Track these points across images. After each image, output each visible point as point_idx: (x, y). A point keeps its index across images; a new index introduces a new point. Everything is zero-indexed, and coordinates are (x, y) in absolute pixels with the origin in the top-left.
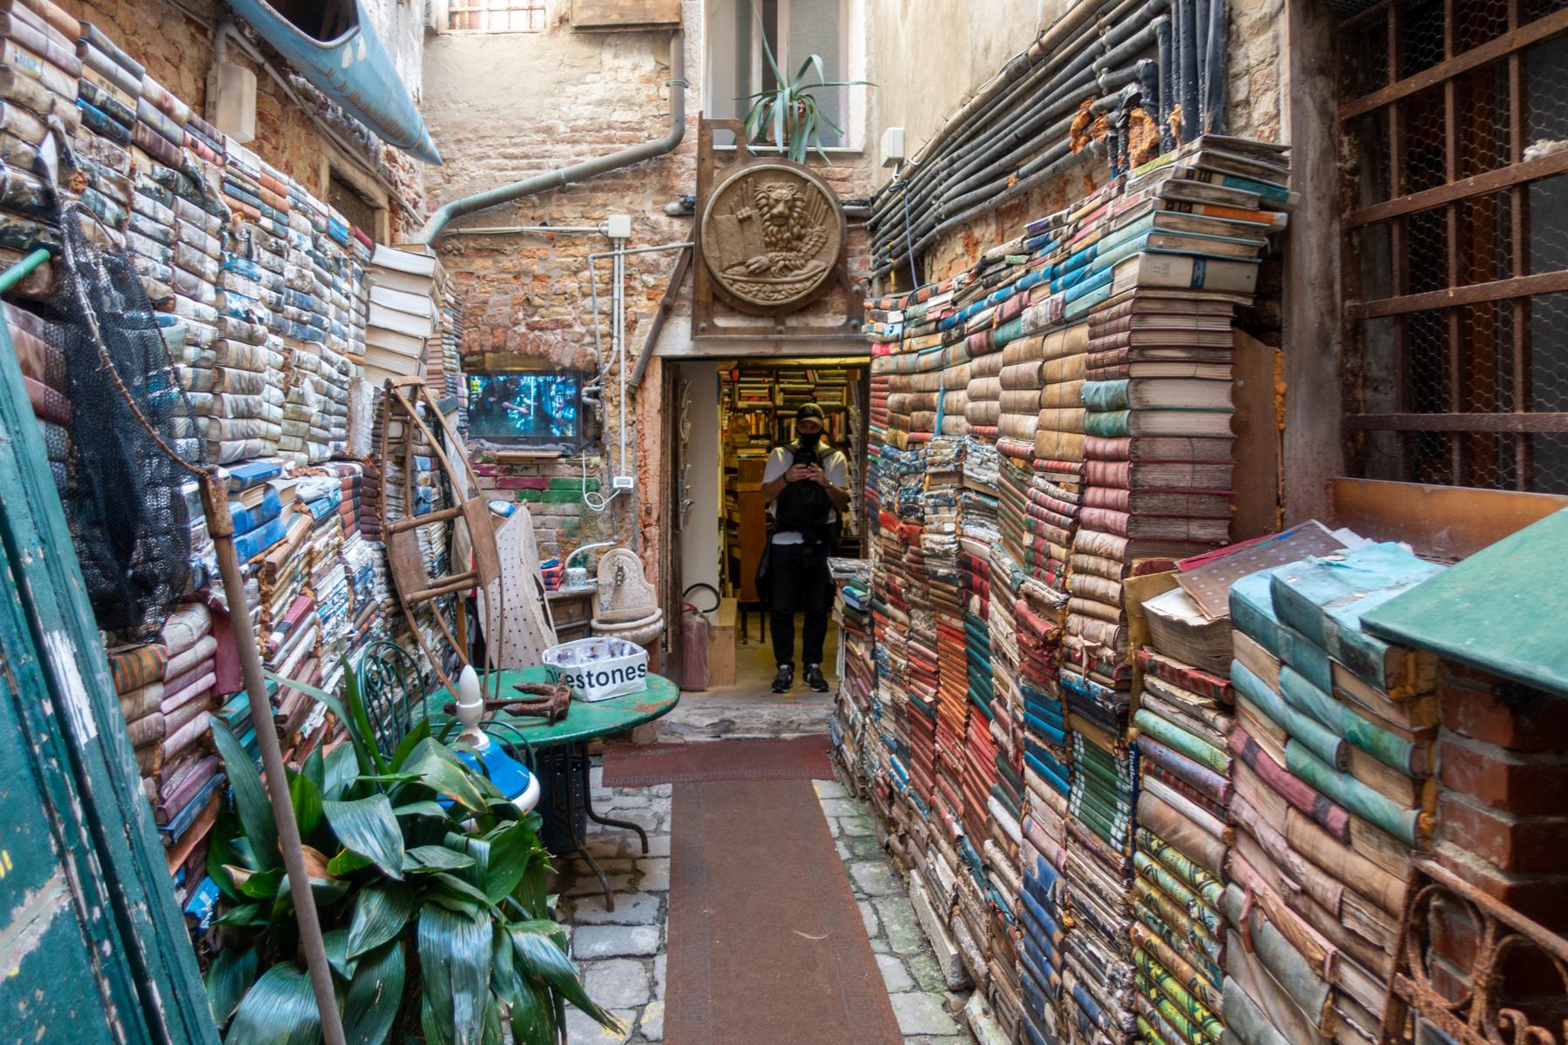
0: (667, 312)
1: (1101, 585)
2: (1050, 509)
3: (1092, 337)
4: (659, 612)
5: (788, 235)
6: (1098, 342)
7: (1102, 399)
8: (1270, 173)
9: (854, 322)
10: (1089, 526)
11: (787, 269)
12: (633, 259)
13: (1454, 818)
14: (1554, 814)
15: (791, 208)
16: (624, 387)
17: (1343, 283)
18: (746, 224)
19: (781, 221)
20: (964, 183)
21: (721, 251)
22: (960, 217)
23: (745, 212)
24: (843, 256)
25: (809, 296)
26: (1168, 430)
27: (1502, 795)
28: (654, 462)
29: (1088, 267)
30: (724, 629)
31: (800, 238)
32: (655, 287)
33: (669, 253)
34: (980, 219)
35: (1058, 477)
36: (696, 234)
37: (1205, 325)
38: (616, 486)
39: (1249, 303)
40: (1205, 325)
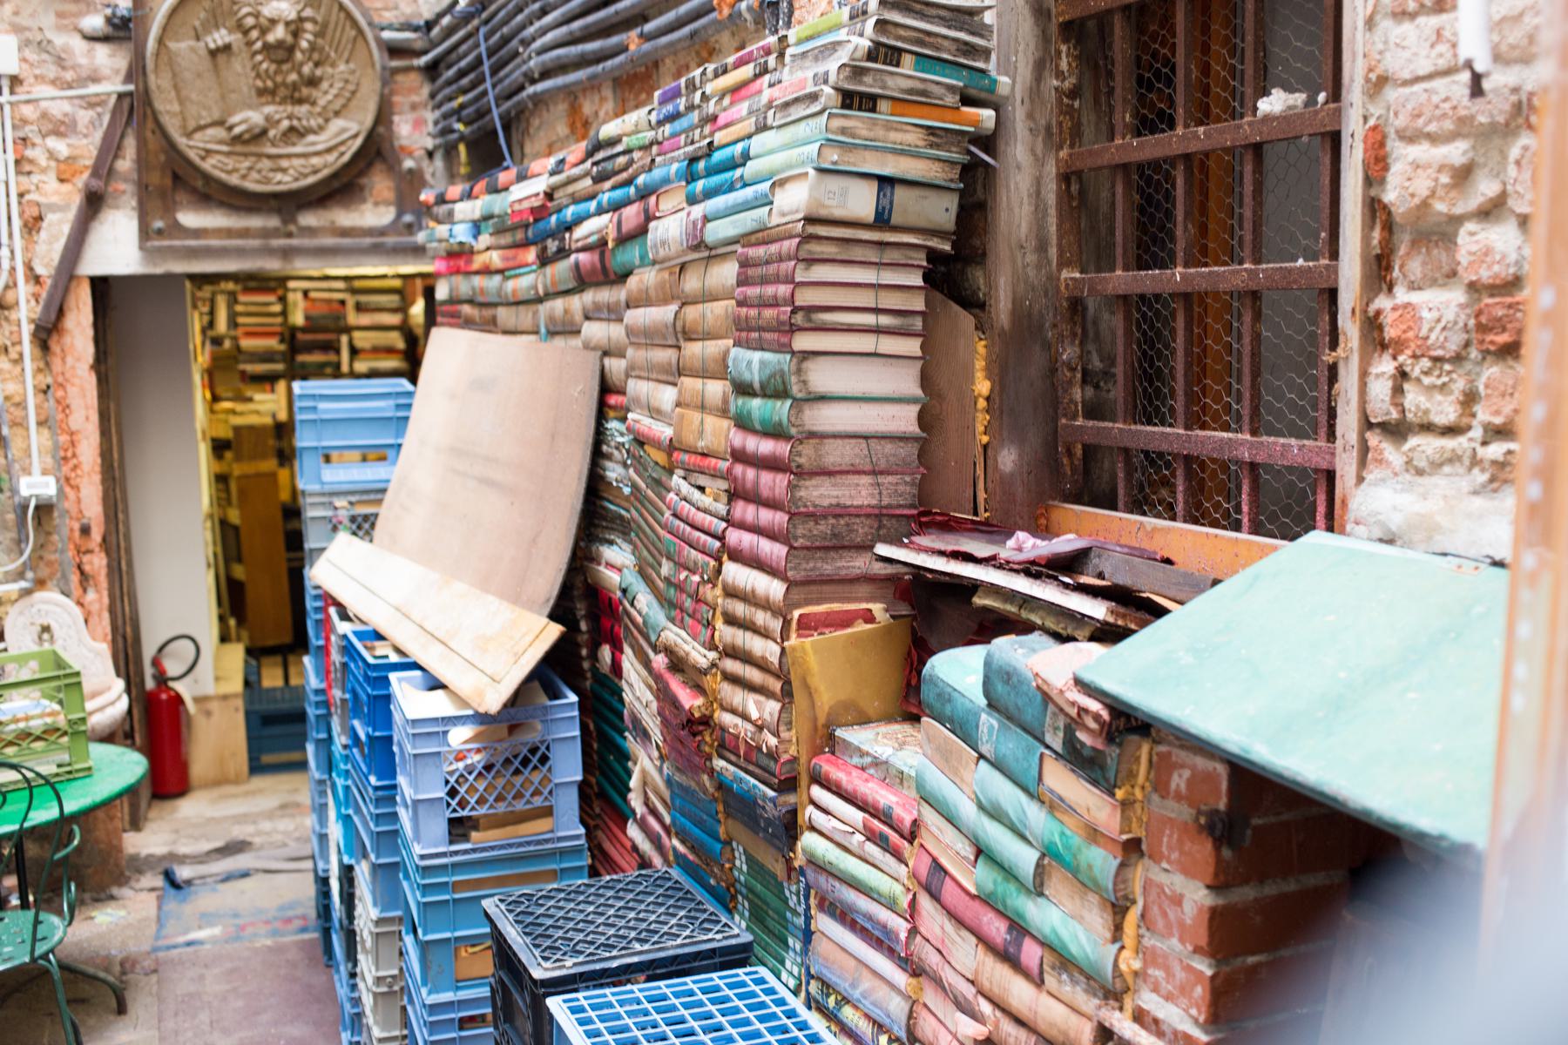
0: (94, 203)
1: (757, 645)
2: (693, 527)
3: (743, 281)
4: (120, 684)
5: (293, 77)
6: (753, 292)
7: (755, 377)
8: (970, 50)
9: (408, 218)
10: (737, 556)
11: (294, 133)
12: (28, 111)
13: (1156, 965)
14: (1253, 953)
15: (296, 34)
16: (27, 330)
17: (1060, 246)
18: (221, 58)
19: (281, 54)
20: (564, 30)
21: (181, 102)
22: (559, 81)
23: (220, 37)
24: (384, 115)
25: (335, 176)
26: (841, 427)
27: (1203, 941)
28: (89, 451)
29: (738, 172)
30: (225, 697)
31: (313, 82)
32: (71, 159)
33: (92, 103)
34: (593, 85)
35: (702, 480)
36: (136, 71)
37: (889, 277)
38: (25, 491)
39: (947, 247)
40: (889, 277)
